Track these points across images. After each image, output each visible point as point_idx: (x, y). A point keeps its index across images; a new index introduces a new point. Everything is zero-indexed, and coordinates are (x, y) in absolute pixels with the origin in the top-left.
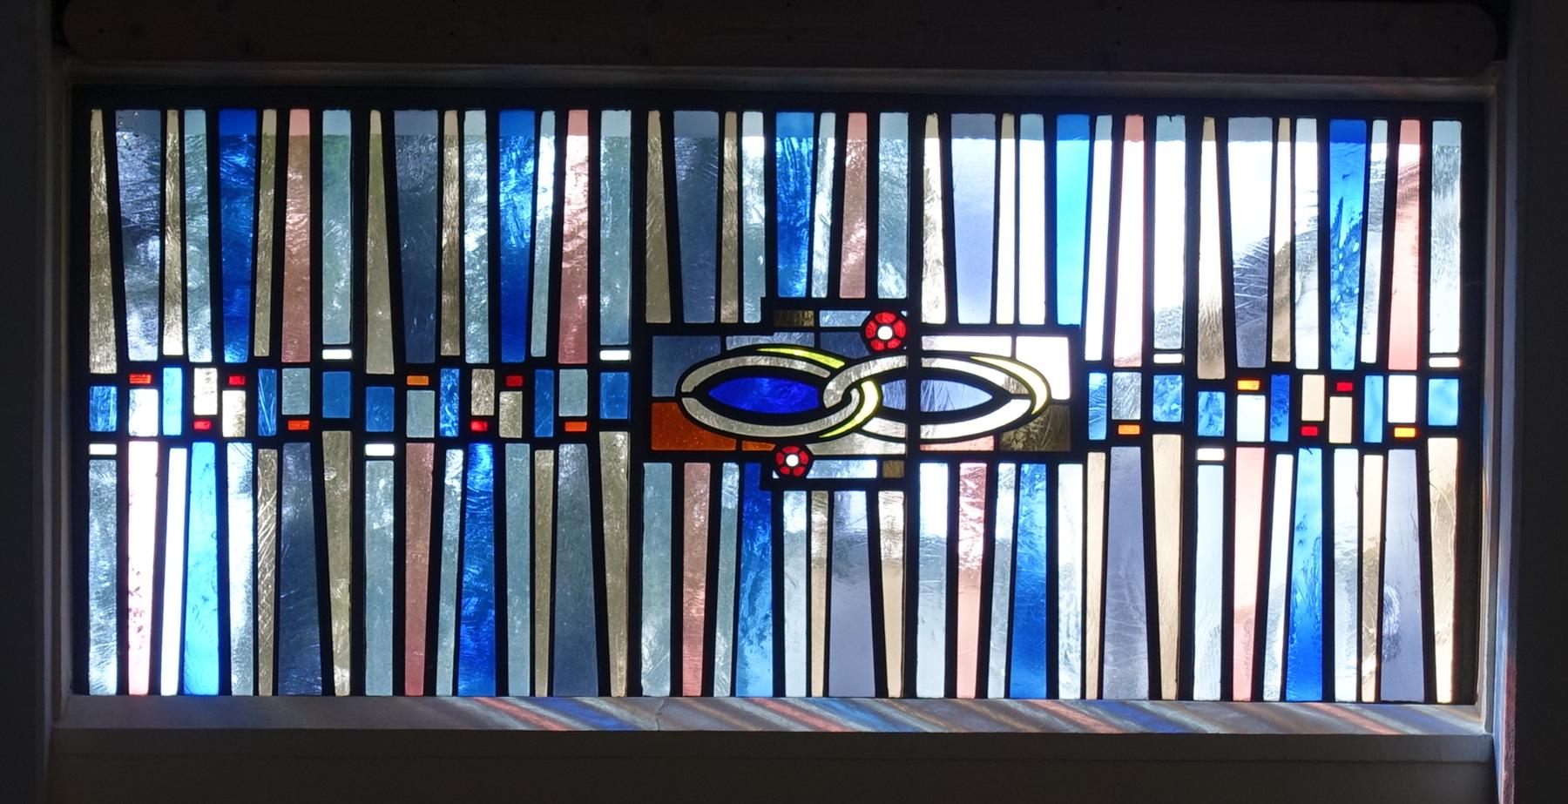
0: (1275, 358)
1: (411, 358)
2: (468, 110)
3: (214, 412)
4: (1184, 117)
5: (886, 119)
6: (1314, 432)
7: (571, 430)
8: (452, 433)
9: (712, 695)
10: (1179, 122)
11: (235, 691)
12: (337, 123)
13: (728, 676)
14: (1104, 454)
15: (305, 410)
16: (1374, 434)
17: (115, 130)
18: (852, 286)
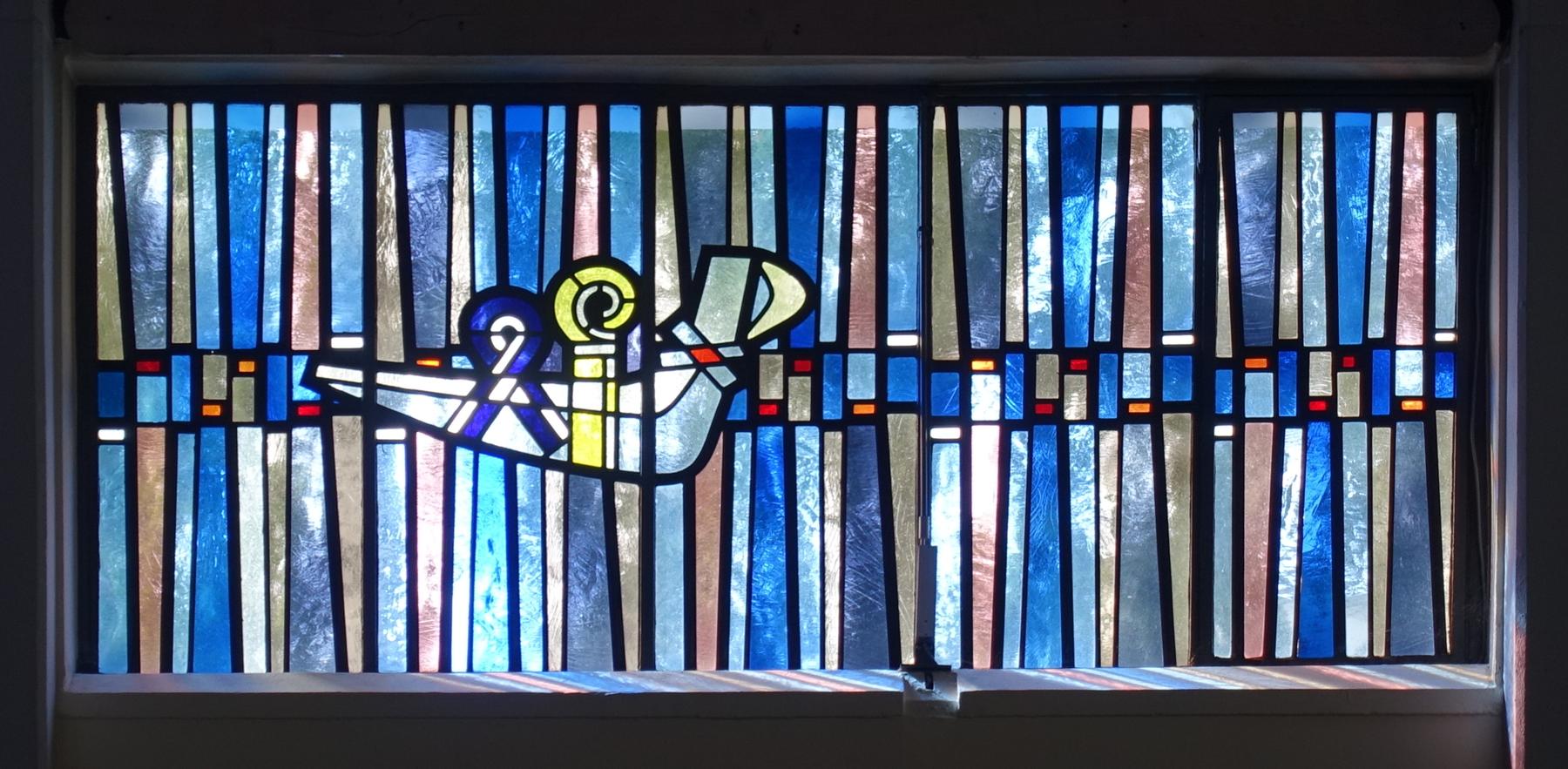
1: (1251, 340)
2: (1108, 104)
5: (337, 111)
6: (216, 411)
7: (286, 415)
8: (1293, 413)
9: (139, 671)
12: (903, 119)
14: (1344, 424)
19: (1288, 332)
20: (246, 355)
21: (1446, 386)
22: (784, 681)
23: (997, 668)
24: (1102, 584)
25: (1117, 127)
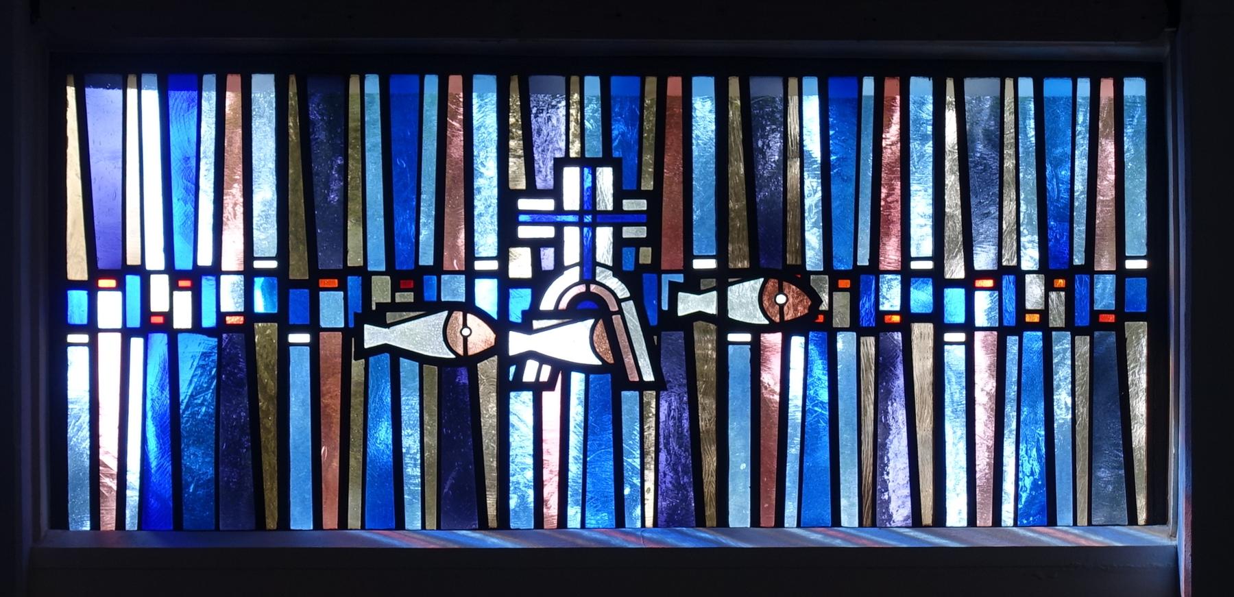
0: (422, 263)
4: (495, 76)
6: (1035, 318)
11: (128, 527)
19: (133, 259)
20: (844, 274)
21: (77, 301)
22: (1044, 538)
23: (61, 528)
25: (680, 94)
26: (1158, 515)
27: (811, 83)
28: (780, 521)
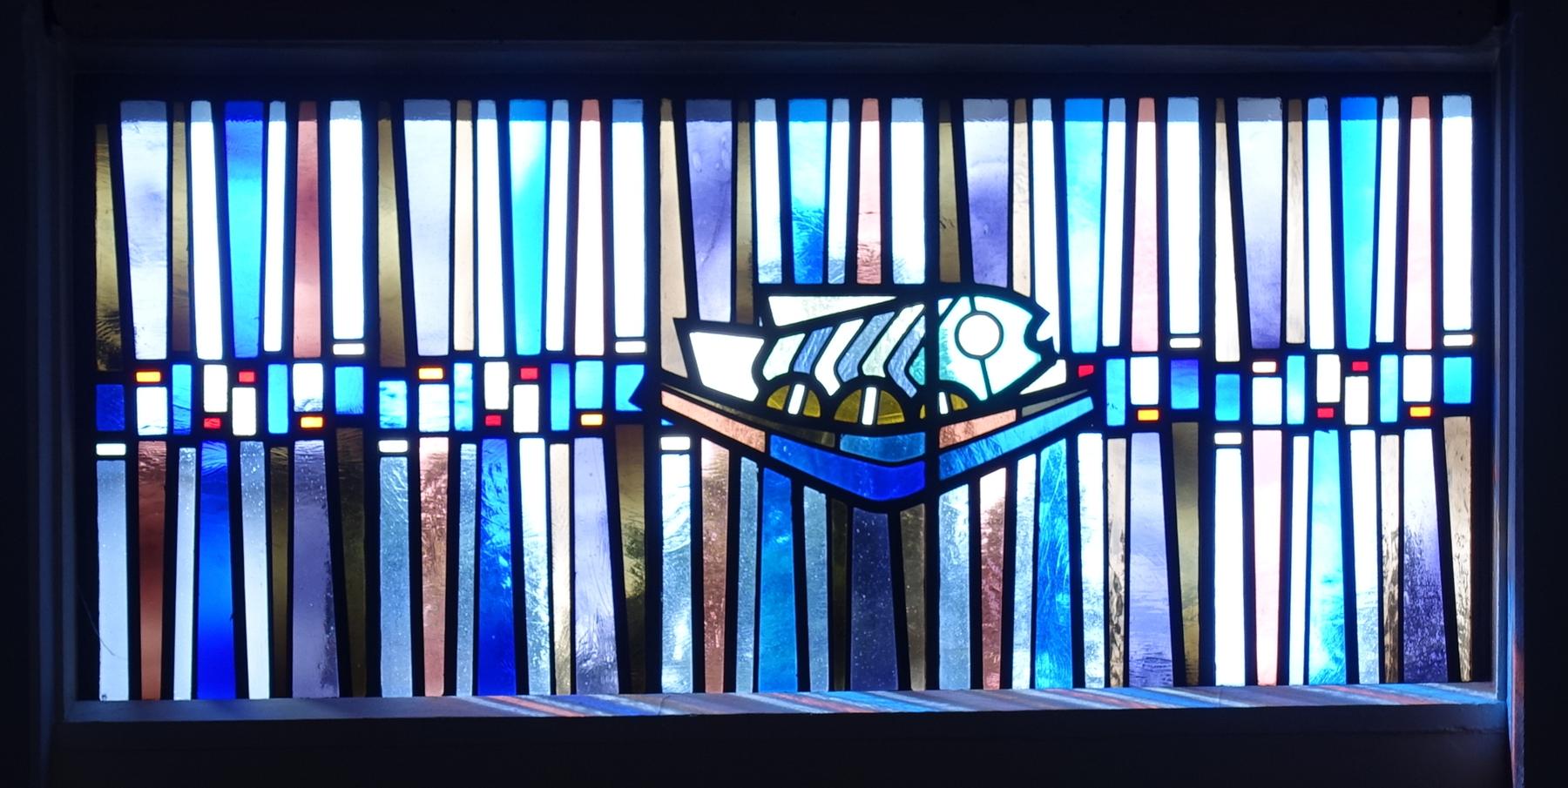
2: (1313, 97)
3: (224, 409)
4: (921, 100)
6: (1329, 413)
10: (1192, 104)
13: (1069, 653)
15: (1154, 399)
16: (1389, 414)
17: (860, 121)
18: (869, 274)
23: (375, 696)
24: (1164, 607)
26: (1482, 673)
27: (1318, 105)
28: (1006, 681)
